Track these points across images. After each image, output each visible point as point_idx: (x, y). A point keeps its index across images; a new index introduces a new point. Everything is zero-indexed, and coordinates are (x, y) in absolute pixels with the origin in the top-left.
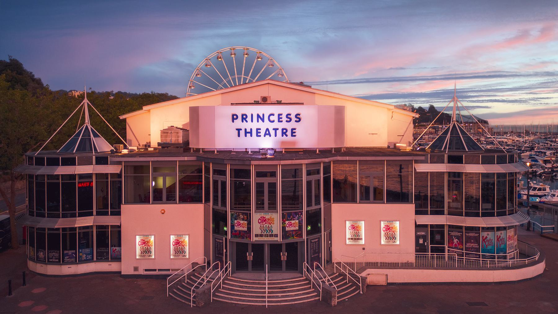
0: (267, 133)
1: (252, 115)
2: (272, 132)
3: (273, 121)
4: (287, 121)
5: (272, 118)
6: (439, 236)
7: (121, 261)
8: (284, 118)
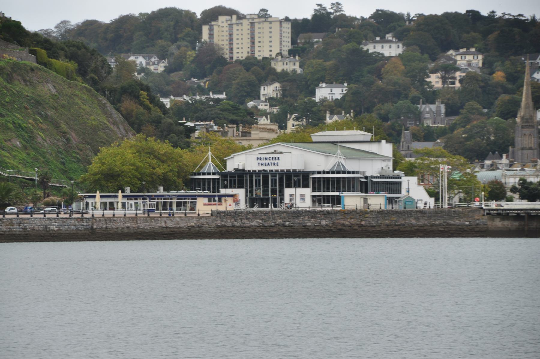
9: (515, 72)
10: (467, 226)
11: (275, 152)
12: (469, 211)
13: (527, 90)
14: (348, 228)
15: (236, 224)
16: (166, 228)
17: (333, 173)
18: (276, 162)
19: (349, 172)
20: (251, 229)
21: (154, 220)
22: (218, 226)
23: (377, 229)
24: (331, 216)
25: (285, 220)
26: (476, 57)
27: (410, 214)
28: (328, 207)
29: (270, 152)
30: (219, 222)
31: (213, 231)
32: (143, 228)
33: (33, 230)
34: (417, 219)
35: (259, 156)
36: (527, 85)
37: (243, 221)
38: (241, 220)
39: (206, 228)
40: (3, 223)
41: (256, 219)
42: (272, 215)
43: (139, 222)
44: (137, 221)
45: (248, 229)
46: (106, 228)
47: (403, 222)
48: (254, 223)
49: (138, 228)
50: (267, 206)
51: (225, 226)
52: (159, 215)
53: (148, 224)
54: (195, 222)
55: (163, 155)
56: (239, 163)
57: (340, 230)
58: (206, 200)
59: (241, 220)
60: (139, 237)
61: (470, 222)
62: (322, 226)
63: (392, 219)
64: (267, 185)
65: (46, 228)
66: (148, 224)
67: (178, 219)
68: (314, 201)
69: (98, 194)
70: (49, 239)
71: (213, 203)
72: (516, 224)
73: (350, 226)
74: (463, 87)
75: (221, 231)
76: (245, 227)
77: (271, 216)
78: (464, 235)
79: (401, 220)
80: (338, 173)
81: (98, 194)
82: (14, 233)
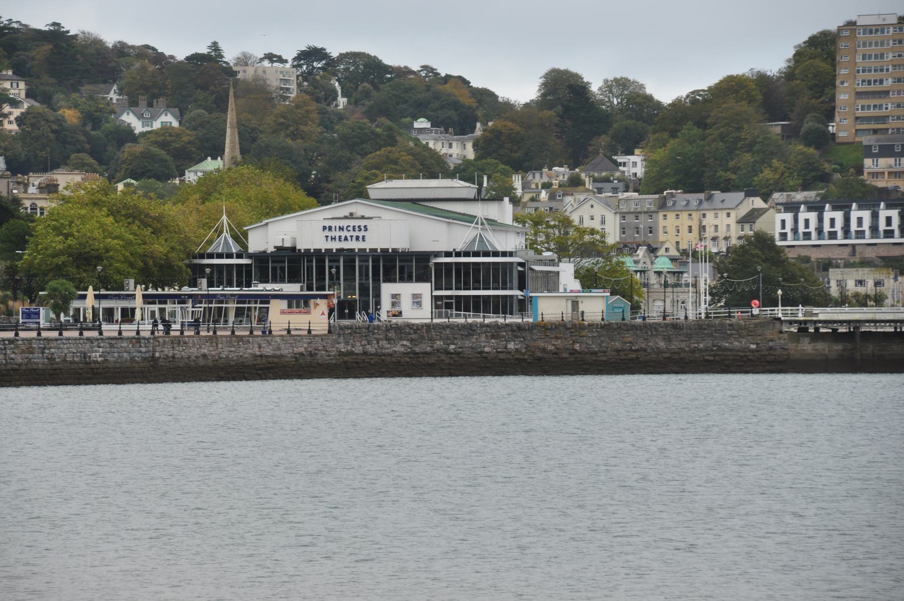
0: (346, 239)
2: (349, 238)
6: (406, 290)
8: (357, 229)
9: (96, 111)
10: (753, 351)
11: (351, 216)
12: (756, 324)
13: (232, 135)
14: (551, 356)
15: (369, 348)
16: (261, 356)
17: (467, 254)
18: (361, 234)
19: (496, 254)
20: (394, 359)
21: (243, 341)
22: (341, 354)
23: (601, 358)
24: (524, 335)
25: (448, 340)
26: (15, 85)
27: (656, 330)
28: (458, 316)
29: (342, 216)
30: (342, 345)
31: (334, 362)
32: (227, 357)
33: (65, 361)
34: (668, 339)
35: (327, 224)
36: (232, 127)
37: (381, 342)
38: (378, 343)
39: (322, 356)
40: (17, 347)
41: (401, 339)
42: (427, 332)
43: (220, 346)
44: (217, 344)
45: (388, 359)
46: (173, 357)
47: (643, 346)
48: (398, 348)
49: (220, 358)
50: (352, 316)
51: (351, 353)
52: (248, 333)
53: (233, 349)
54: (305, 345)
55: (154, 218)
56: (284, 237)
57: (539, 359)
58: (284, 304)
59: (378, 343)
60: (222, 374)
61: (757, 344)
62: (509, 353)
63: (626, 340)
64: (357, 275)
65: (85, 358)
66: (233, 349)
67: (278, 339)
68: (437, 307)
69: (90, 293)
70: (89, 379)
71: (295, 309)
72: (839, 347)
73: (556, 353)
74: (23, 130)
75: (346, 362)
76: (384, 355)
77: (426, 335)
78: (749, 369)
79: (641, 340)
80: (476, 254)
81: (90, 293)
82: (35, 367)
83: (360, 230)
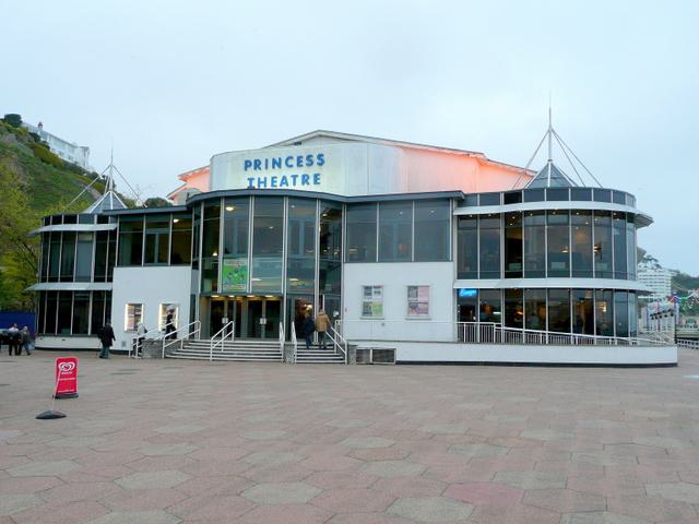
1: (267, 161)
3: (291, 166)
4: (308, 165)
5: (290, 162)
6: (392, 277)
7: (461, 340)
8: (305, 162)
83: (311, 164)
